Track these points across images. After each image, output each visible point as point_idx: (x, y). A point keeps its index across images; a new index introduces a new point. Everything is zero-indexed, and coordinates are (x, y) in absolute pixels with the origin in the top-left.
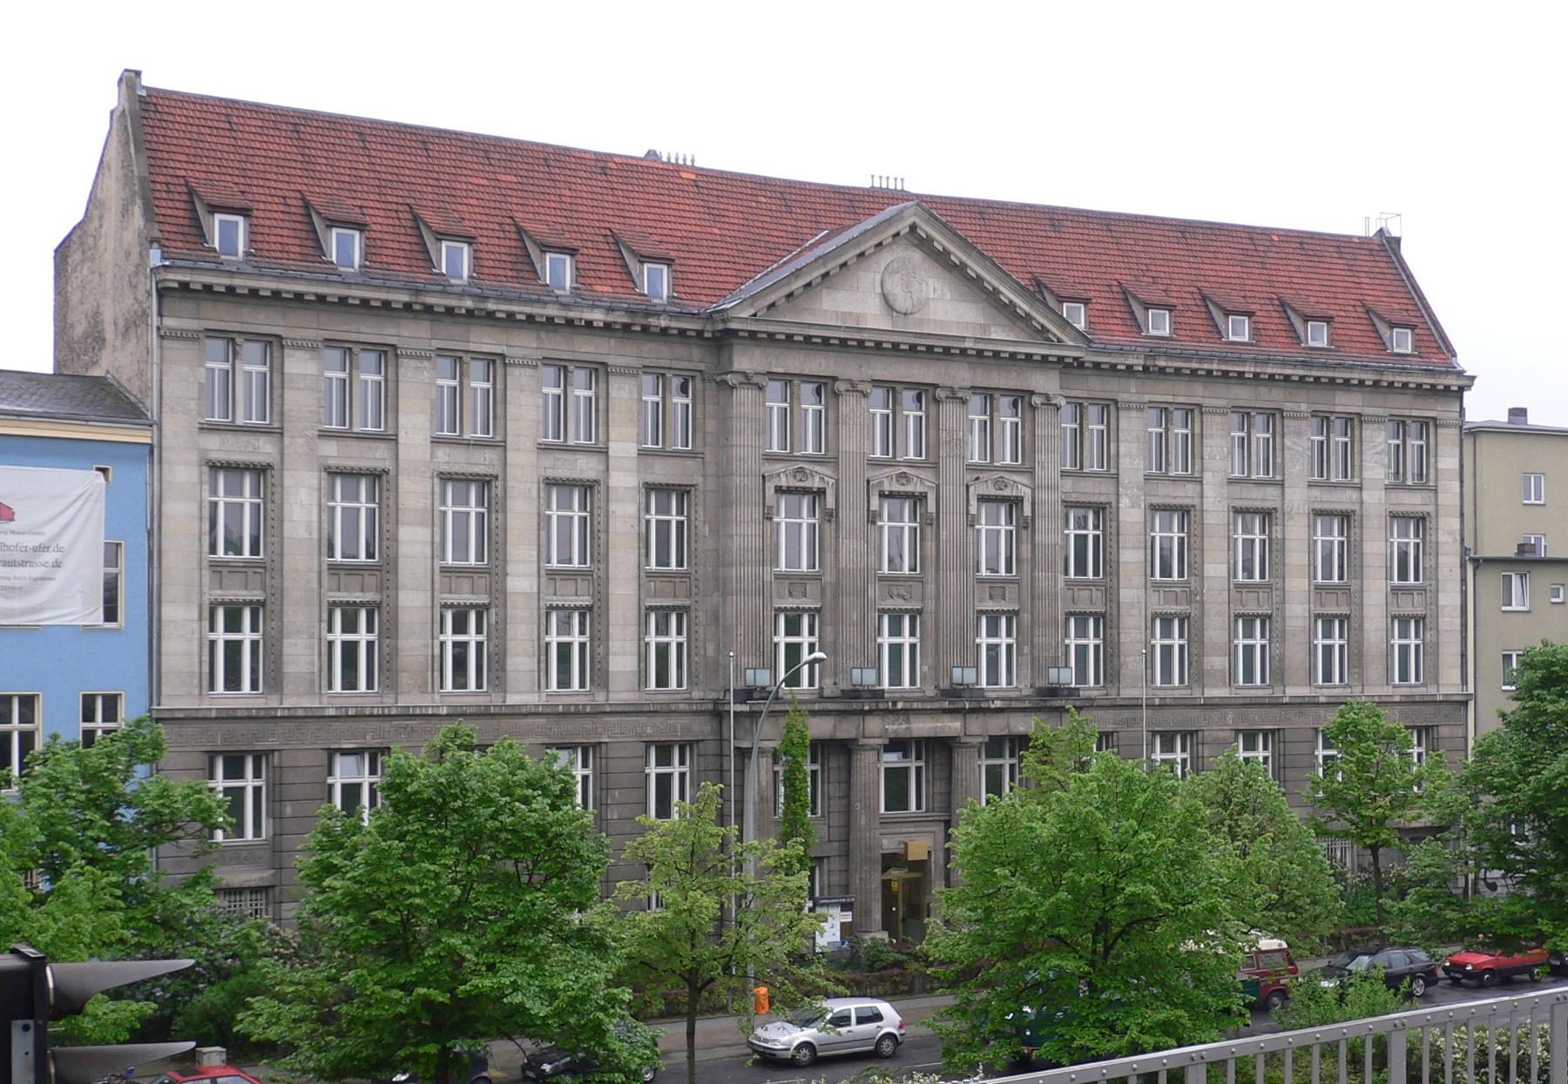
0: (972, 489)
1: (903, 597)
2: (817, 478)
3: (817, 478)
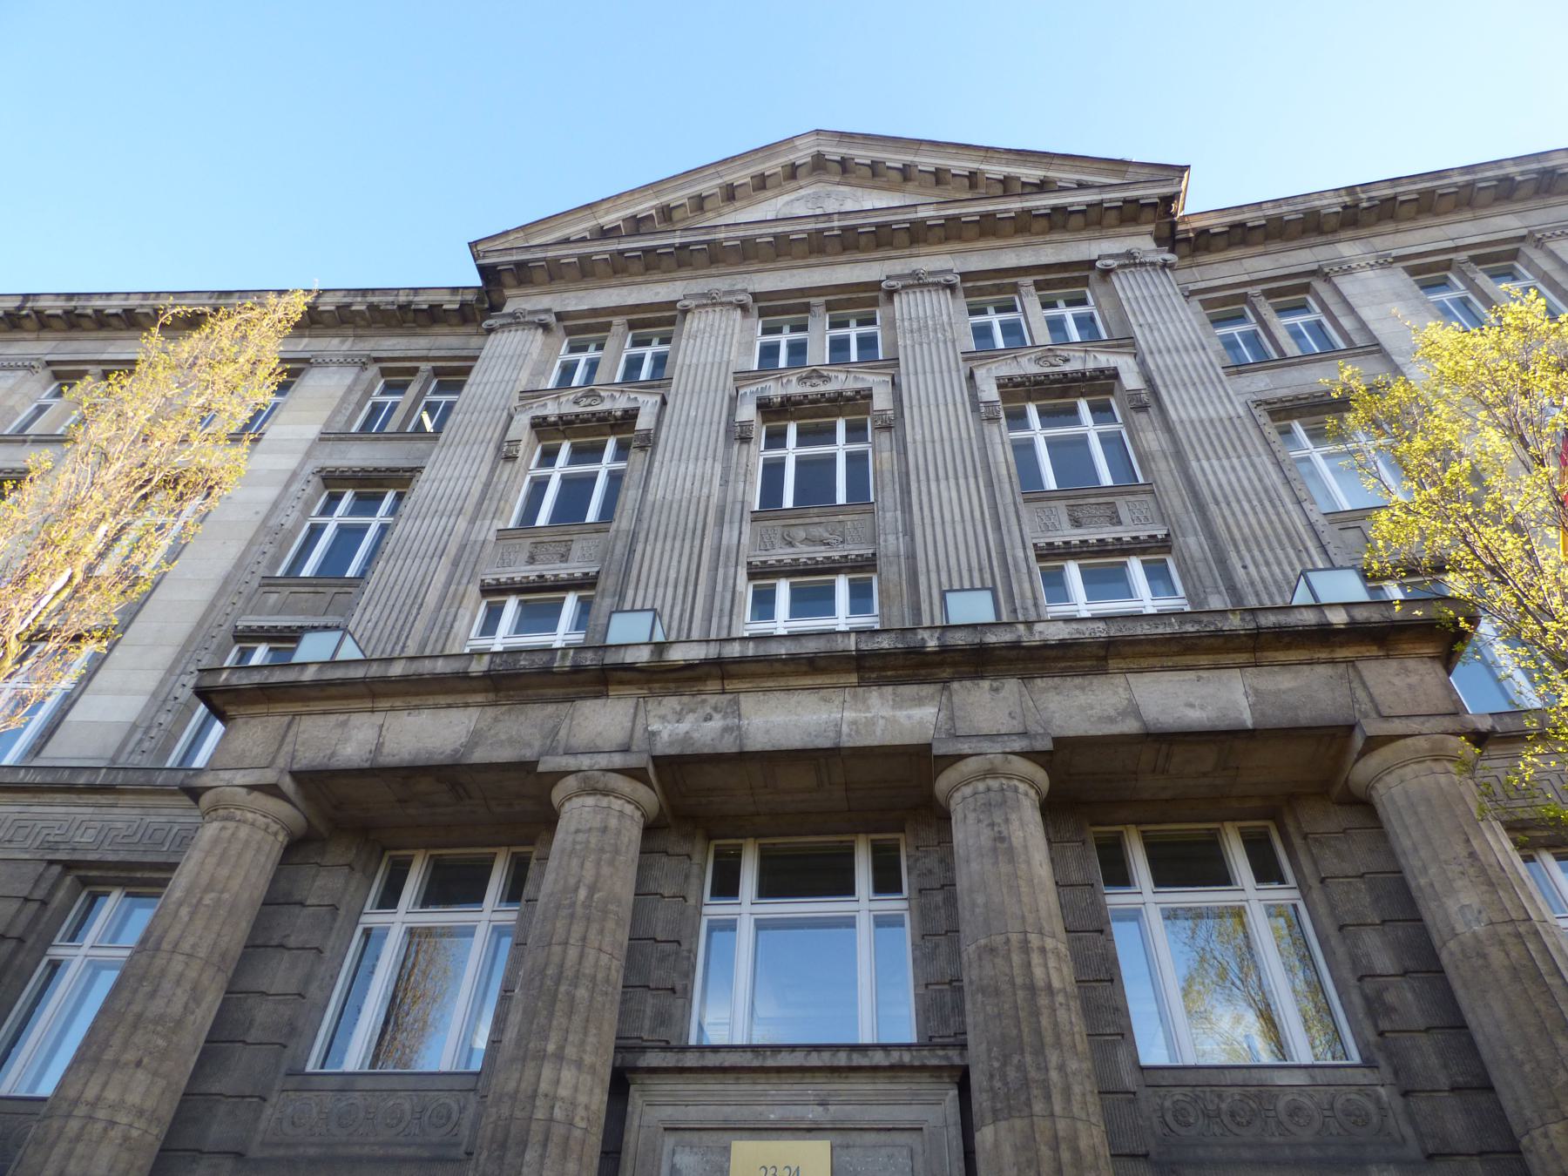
0: (980, 374)
1: (823, 543)
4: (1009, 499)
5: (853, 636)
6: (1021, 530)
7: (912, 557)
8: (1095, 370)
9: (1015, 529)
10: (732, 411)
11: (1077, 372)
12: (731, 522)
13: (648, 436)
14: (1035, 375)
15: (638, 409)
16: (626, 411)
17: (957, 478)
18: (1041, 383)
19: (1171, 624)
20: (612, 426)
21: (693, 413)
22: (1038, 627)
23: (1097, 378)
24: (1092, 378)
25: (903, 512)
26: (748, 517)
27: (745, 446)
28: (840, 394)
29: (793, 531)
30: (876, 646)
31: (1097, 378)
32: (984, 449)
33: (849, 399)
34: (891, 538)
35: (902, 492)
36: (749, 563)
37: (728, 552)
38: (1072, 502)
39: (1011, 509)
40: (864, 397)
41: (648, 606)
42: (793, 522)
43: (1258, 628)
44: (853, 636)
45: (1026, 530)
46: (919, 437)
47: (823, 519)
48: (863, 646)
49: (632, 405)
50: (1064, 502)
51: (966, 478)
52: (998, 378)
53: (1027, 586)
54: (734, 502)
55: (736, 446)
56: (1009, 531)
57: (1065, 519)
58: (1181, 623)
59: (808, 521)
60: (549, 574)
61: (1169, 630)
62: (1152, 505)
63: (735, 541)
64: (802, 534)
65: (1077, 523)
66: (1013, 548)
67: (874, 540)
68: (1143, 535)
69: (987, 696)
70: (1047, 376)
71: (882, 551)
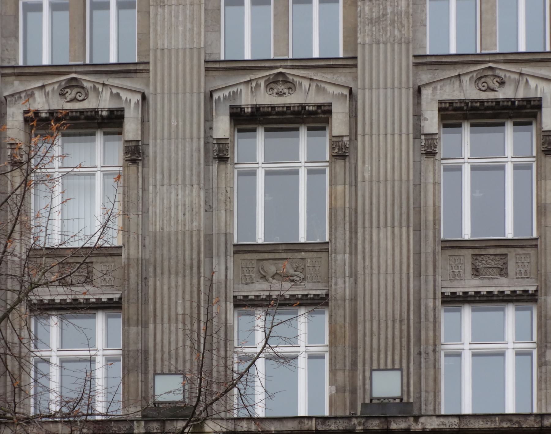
0: (427, 93)
2: (106, 95)
3: (106, 95)
4: (430, 250)
5: (314, 420)
6: (435, 281)
7: (354, 299)
8: (523, 100)
9: (431, 278)
10: (209, 129)
11: (508, 100)
12: (218, 256)
13: (137, 147)
14: (473, 101)
15: (122, 110)
16: (111, 111)
17: (393, 227)
18: (476, 109)
19: (495, 421)
20: (98, 123)
21: (174, 124)
22: (422, 420)
23: (524, 107)
24: (520, 107)
25: (350, 254)
26: (231, 250)
27: (223, 166)
28: (303, 107)
29: (266, 264)
30: (327, 428)
31: (524, 107)
32: (418, 186)
33: (311, 113)
34: (340, 281)
35: (350, 232)
36: (235, 297)
37: (218, 288)
38: (477, 252)
39: (430, 259)
40: (324, 112)
41: (180, 368)
42: (266, 256)
43: (542, 427)
44: (314, 420)
45: (439, 278)
46: (367, 175)
47: (289, 255)
48: (320, 428)
49: (114, 105)
50: (471, 252)
51: (401, 227)
52: (441, 102)
53: (431, 334)
54: (219, 234)
55: (215, 166)
56: (426, 281)
57: (468, 268)
58: (501, 421)
59: (277, 256)
60: (81, 298)
61: (493, 426)
62: (533, 260)
63: (223, 277)
64: (272, 268)
65: (476, 272)
66: (427, 297)
67: (327, 281)
68: (519, 289)
69: (427, 122)
70: (482, 102)
71: (332, 293)
